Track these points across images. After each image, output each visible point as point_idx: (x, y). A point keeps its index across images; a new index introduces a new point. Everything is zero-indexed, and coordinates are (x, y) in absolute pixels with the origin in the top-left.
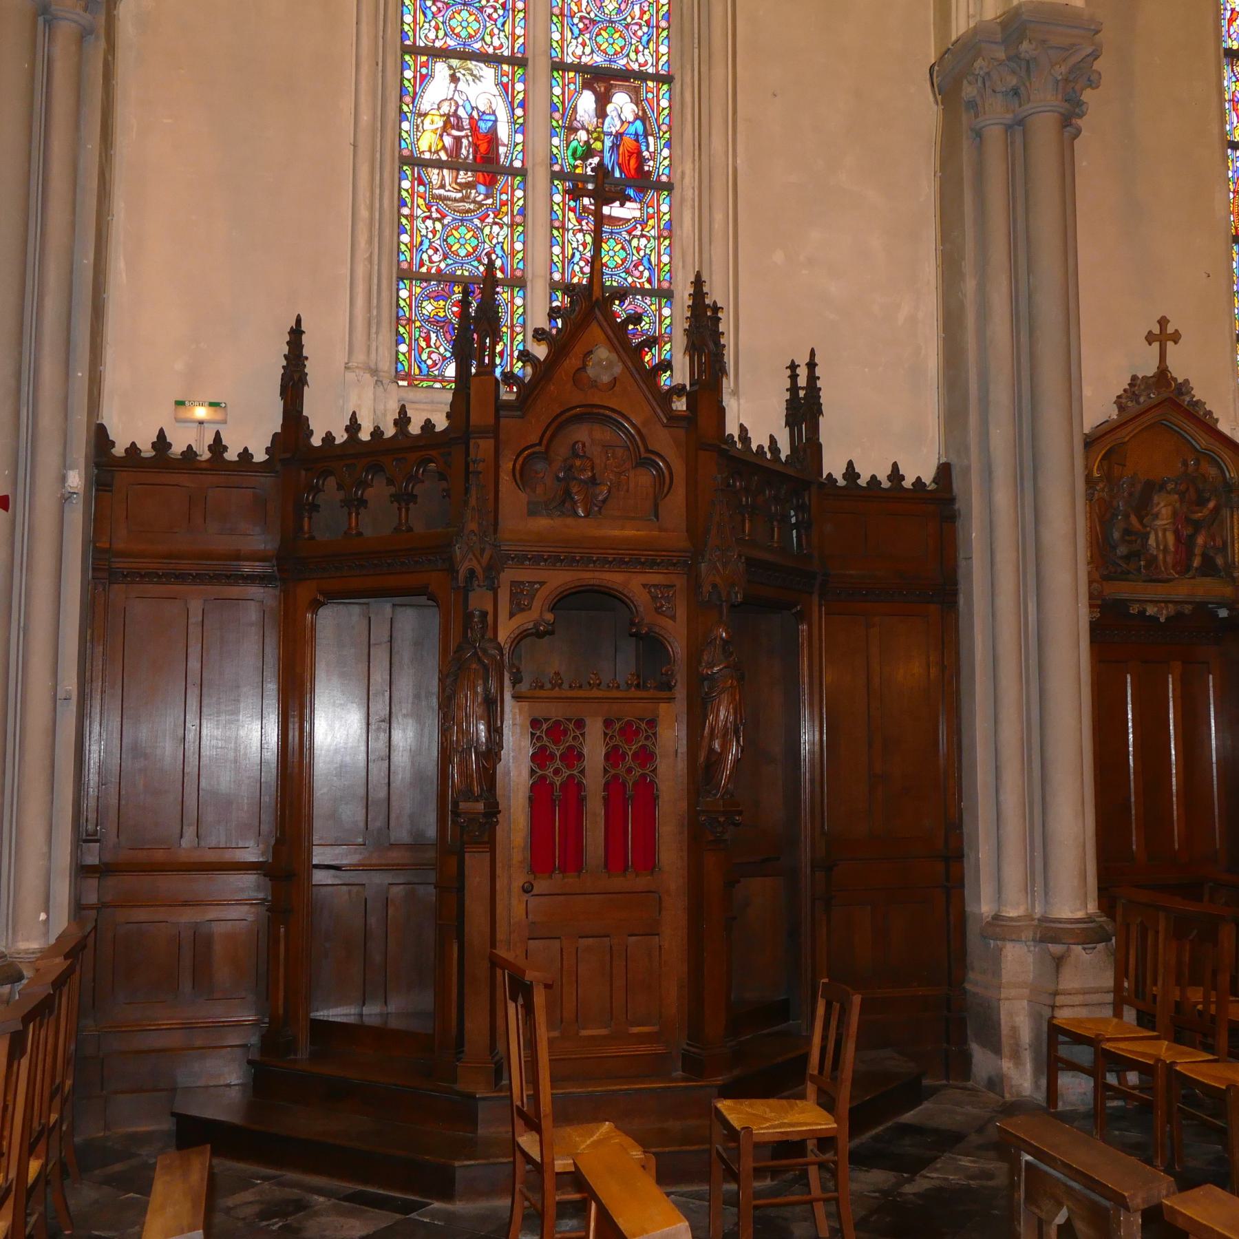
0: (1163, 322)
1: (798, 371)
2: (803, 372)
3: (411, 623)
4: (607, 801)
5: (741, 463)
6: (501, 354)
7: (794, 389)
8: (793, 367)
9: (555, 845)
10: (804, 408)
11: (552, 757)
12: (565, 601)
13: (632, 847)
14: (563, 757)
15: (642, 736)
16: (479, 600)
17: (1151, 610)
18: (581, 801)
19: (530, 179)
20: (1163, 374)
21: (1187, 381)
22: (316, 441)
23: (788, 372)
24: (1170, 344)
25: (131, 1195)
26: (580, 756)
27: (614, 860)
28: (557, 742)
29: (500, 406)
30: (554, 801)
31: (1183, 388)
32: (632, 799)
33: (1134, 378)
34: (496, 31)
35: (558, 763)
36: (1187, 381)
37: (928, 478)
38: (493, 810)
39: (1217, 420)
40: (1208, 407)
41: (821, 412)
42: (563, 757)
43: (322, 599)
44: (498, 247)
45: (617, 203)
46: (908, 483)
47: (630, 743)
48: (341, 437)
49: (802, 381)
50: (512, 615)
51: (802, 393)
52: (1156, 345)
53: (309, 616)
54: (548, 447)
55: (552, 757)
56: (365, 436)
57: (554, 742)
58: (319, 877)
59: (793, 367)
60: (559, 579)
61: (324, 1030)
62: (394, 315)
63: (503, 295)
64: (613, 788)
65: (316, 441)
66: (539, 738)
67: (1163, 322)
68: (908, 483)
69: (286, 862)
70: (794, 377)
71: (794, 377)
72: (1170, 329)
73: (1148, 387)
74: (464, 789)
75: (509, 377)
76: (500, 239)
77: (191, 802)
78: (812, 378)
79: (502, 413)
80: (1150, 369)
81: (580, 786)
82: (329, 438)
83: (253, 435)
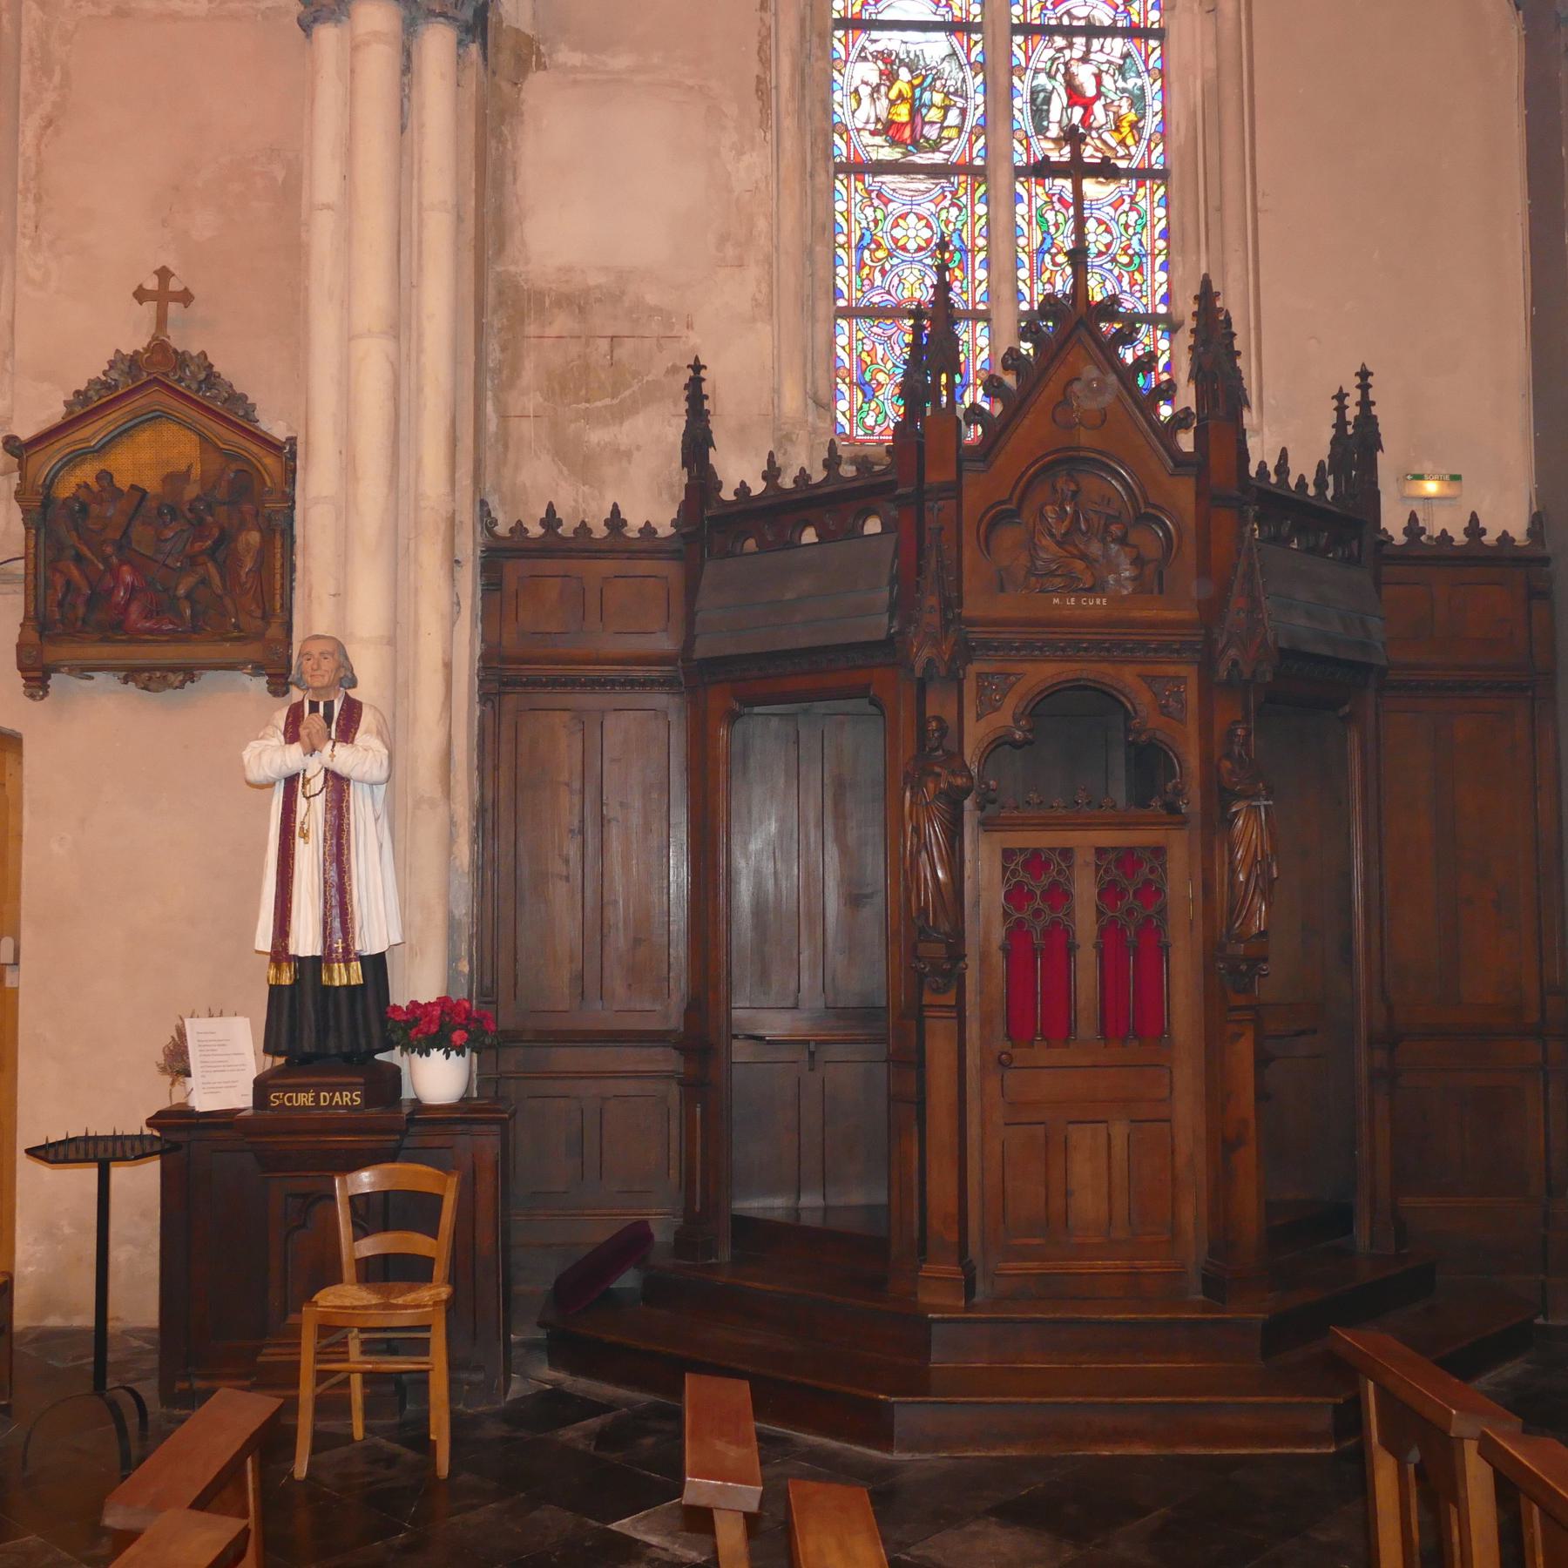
1: (1347, 401)
2: (1355, 396)
3: (857, 741)
4: (1102, 955)
5: (1276, 502)
7: (1340, 424)
8: (1341, 396)
9: (1036, 1006)
10: (1357, 444)
11: (1031, 896)
12: (1047, 707)
13: (1134, 1011)
14: (1046, 896)
15: (1146, 869)
16: (938, 705)
18: (1069, 950)
19: (994, 321)
20: (159, 346)
22: (727, 494)
23: (1335, 403)
26: (1067, 896)
27: (1112, 1025)
28: (1037, 877)
29: (966, 457)
30: (1036, 953)
32: (1134, 952)
35: (1038, 903)
37: (1519, 530)
38: (956, 952)
41: (1379, 446)
42: (1046, 896)
43: (736, 706)
44: (955, 236)
46: (1490, 538)
47: (1129, 877)
48: (757, 487)
49: (1352, 412)
50: (979, 717)
51: (1350, 430)
52: (150, 308)
53: (722, 732)
54: (1020, 506)
55: (1031, 896)
56: (787, 482)
57: (1035, 882)
58: (741, 1052)
59: (1341, 396)
60: (1042, 673)
61: (746, 1227)
63: (963, 331)
64: (1110, 936)
65: (727, 494)
66: (1014, 873)
68: (1490, 538)
69: (701, 1039)
70: (1341, 410)
71: (1341, 410)
72: (174, 285)
74: (924, 940)
75: (975, 412)
76: (959, 225)
78: (1365, 404)
79: (966, 465)
81: (1067, 933)
82: (743, 489)
83: (649, 501)
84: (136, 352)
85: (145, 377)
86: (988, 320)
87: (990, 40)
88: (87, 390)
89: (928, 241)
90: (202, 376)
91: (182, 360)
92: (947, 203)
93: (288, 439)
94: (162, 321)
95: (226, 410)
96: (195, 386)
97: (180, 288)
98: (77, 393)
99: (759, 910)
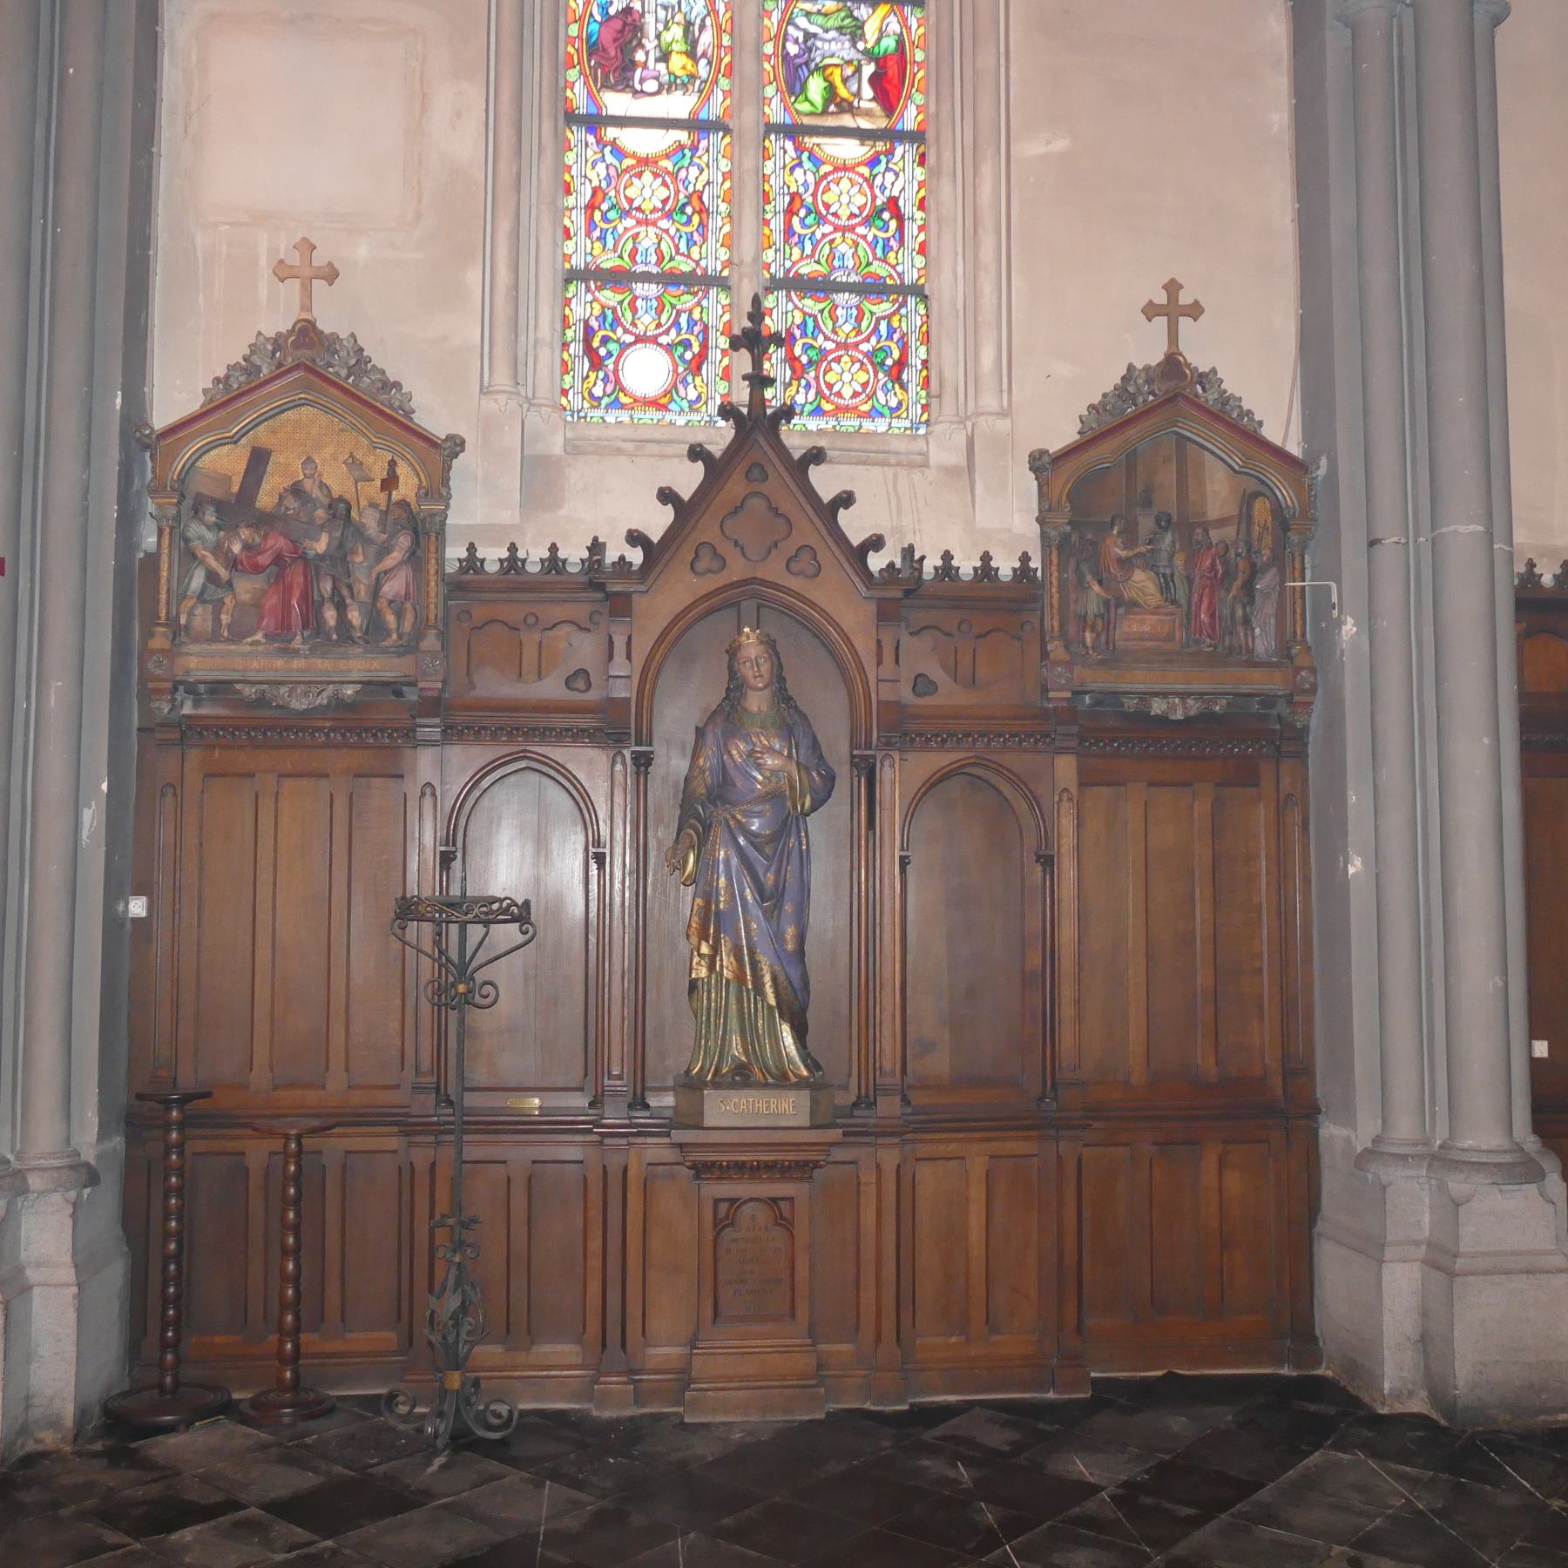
0: (1172, 287)
6: (167, 1236)
10: (696, 453)
17: (1158, 707)
20: (1173, 365)
21: (1214, 371)
24: (1185, 323)
25: (1160, 1373)
31: (1206, 379)
33: (1131, 367)
34: (604, 185)
36: (1214, 371)
39: (1261, 423)
40: (1246, 406)
45: (569, 93)
52: (1161, 322)
62: (558, 361)
67: (1172, 287)
72: (1185, 299)
73: (1149, 381)
77: (890, 969)
80: (1153, 355)
84: (279, 335)
85: (289, 362)
86: (925, 298)
87: (932, 19)
88: (227, 377)
89: (862, 209)
90: (353, 362)
91: (330, 343)
92: (686, 162)
93: (450, 438)
94: (307, 306)
95: (375, 405)
96: (344, 373)
97: (1190, 301)
98: (217, 380)
99: (136, 1450)
